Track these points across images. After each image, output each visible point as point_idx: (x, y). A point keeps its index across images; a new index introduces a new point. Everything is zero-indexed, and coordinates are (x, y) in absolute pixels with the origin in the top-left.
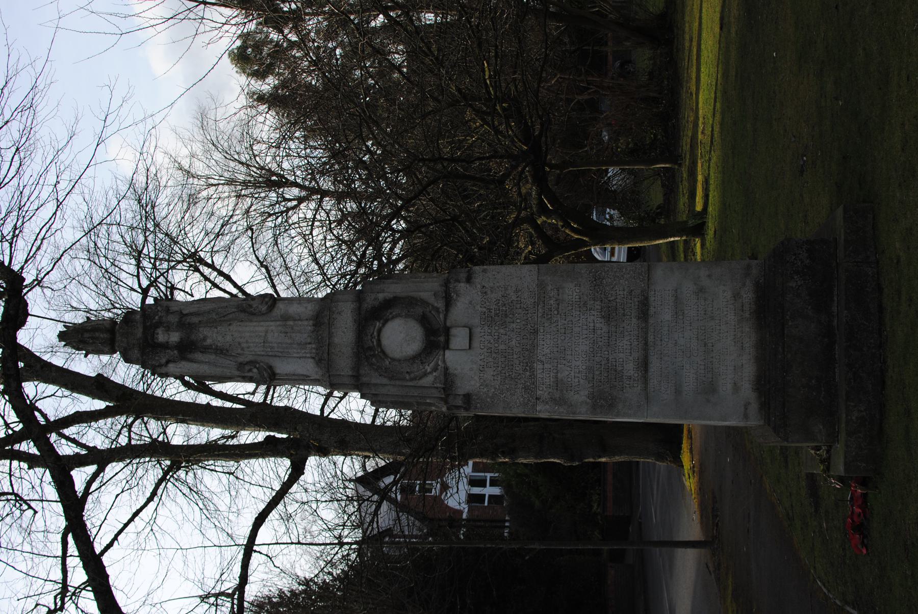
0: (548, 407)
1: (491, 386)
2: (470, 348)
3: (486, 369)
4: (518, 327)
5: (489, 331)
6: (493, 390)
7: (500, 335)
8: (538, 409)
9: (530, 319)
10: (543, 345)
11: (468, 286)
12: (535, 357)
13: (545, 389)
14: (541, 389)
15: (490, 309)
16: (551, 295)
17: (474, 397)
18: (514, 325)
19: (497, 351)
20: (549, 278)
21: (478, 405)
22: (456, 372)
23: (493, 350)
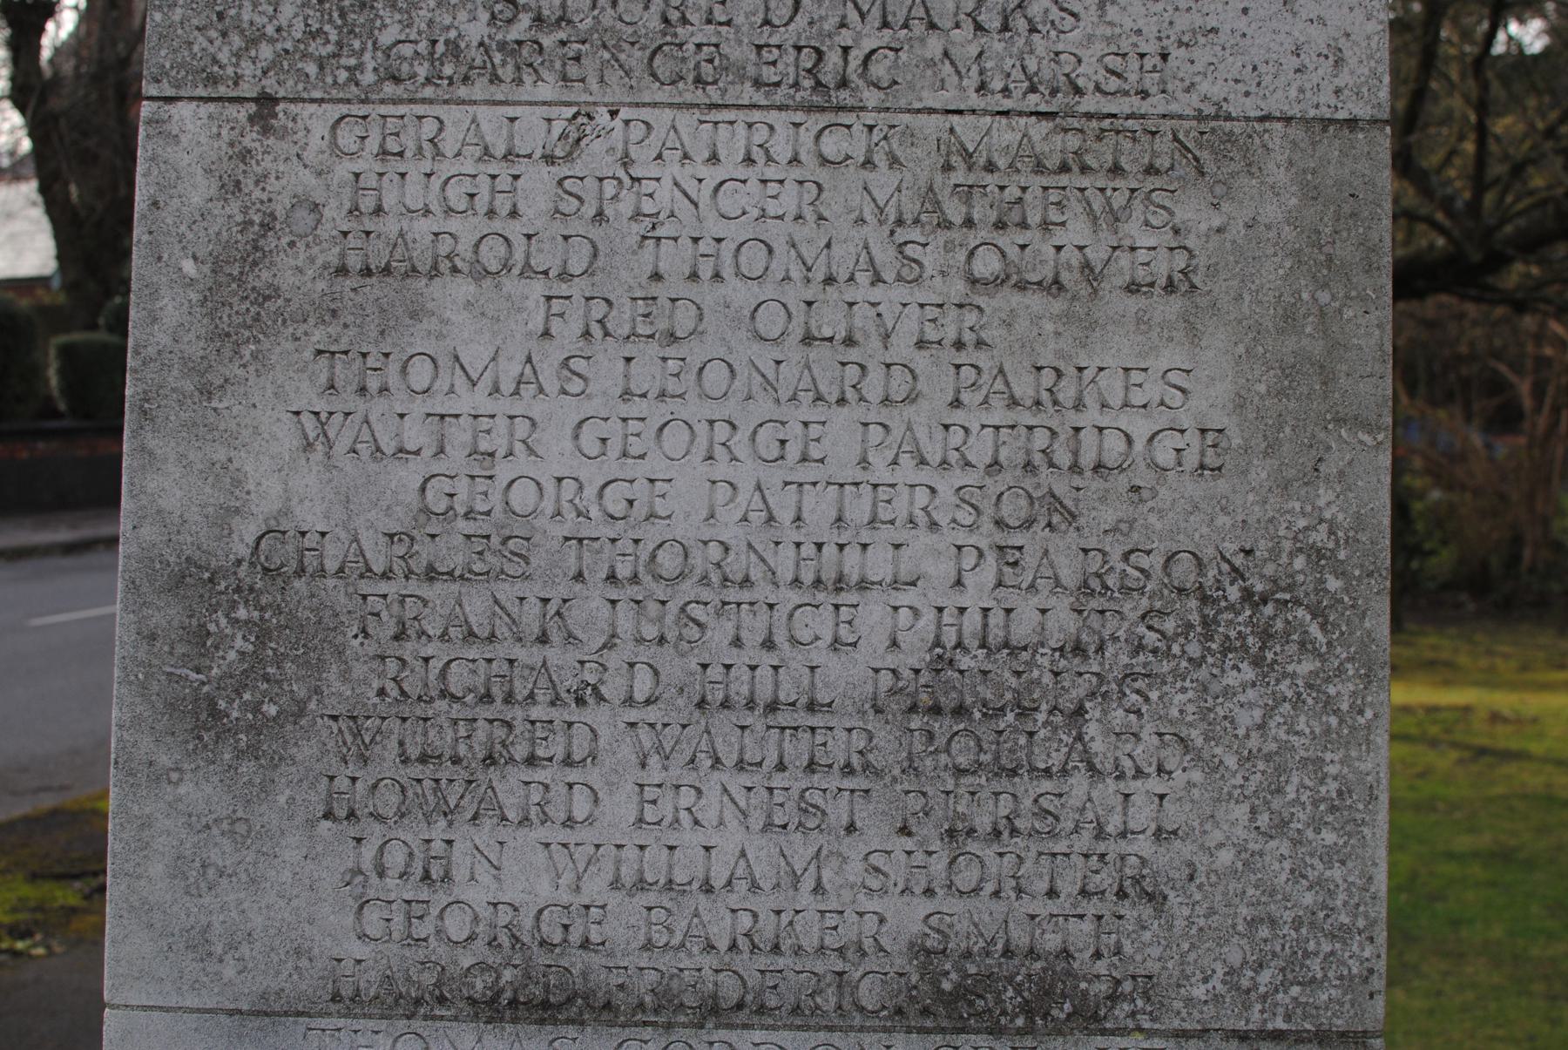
0: (196, 199)
8: (183, 110)
9: (934, 45)
10: (714, 158)
12: (616, 94)
13: (344, 169)
14: (347, 139)
16: (1133, 230)
20: (1271, 212)
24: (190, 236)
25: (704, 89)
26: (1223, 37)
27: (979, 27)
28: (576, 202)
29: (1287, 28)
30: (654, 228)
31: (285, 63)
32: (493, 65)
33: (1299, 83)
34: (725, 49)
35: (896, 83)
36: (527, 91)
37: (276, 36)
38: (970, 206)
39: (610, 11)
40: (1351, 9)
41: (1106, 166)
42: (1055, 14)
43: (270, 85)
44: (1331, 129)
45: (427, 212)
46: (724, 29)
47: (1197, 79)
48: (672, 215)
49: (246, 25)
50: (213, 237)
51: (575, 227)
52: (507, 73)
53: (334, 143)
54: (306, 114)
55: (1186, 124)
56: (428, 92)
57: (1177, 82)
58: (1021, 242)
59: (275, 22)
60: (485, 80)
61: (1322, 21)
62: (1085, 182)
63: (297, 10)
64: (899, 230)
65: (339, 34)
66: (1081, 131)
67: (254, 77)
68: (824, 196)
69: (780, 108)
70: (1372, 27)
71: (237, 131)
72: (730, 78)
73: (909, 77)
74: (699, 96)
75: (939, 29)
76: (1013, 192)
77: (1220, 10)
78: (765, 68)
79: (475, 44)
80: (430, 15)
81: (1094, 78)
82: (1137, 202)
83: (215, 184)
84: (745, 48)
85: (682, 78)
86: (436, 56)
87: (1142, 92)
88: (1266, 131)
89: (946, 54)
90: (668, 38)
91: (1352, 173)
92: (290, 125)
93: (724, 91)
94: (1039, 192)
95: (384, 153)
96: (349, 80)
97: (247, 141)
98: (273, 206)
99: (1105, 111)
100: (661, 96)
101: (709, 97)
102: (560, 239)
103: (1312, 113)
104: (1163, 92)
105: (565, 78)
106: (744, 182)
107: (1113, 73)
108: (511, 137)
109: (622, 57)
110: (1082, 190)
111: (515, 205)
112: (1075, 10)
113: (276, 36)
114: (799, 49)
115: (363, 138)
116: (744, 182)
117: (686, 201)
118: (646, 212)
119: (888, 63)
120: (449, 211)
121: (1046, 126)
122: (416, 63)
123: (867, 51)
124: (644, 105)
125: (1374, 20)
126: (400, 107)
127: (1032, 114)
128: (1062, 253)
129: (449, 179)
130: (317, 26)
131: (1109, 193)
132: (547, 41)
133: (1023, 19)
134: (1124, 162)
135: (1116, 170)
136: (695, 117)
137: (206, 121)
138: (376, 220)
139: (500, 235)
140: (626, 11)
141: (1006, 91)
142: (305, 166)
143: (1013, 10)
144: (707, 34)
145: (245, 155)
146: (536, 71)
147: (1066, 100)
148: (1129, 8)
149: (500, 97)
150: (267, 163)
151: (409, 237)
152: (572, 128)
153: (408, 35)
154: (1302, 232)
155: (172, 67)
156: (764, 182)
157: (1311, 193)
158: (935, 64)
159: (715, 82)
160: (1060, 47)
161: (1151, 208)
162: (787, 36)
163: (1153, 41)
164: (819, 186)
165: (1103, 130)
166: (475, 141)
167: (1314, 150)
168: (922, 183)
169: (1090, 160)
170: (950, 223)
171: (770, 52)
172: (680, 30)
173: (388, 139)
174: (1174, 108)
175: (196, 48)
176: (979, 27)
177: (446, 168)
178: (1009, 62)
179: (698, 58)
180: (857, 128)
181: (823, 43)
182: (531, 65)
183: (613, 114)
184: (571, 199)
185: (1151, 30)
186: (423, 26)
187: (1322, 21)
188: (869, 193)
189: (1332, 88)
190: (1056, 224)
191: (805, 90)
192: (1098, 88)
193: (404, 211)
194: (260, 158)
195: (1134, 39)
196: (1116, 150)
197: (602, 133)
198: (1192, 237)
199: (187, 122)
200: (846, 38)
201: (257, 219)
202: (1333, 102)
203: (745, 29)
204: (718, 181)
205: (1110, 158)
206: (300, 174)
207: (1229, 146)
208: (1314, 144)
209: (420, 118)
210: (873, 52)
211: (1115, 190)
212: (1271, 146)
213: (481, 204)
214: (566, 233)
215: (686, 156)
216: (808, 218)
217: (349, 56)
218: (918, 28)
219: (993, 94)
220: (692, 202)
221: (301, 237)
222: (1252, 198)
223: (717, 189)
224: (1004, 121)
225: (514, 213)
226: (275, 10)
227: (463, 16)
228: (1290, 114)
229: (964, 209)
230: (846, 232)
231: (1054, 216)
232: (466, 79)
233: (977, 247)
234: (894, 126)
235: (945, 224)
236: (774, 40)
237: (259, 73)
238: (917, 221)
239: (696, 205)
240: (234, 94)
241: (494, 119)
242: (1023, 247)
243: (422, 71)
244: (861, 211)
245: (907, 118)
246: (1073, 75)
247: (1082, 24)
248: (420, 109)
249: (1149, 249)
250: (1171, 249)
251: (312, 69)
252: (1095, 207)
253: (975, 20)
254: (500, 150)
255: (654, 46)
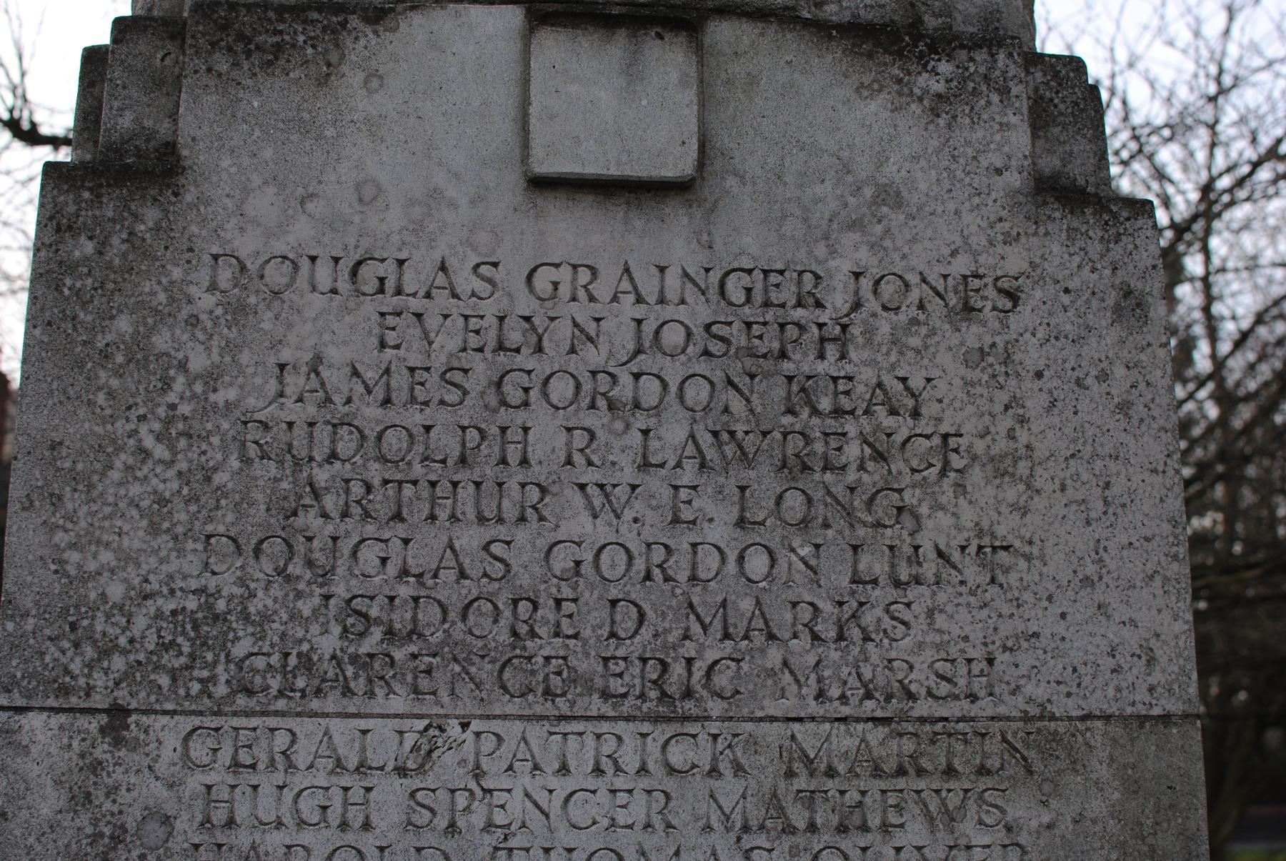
0: (46, 811)
1: (231, 348)
2: (541, 184)
3: (370, 307)
4: (709, 562)
5: (673, 336)
6: (198, 362)
7: (641, 421)
8: (34, 721)
9: (774, 656)
10: (564, 769)
11: (1014, 179)
12: (467, 706)
13: (195, 782)
14: (199, 751)
15: (843, 341)
16: (967, 828)
17: (152, 215)
18: (720, 531)
19: (514, 396)
20: (1096, 806)
21: (89, 247)
22: (357, 79)
23: (525, 360)
24: (38, 848)
25: (553, 701)
26: (1044, 641)
27: (815, 637)
28: (427, 814)
29: (1102, 631)
30: (506, 839)
31: (138, 675)
32: (345, 678)
33: (1115, 682)
34: (573, 662)
35: (738, 692)
36: (380, 703)
37: (128, 647)
38: (813, 811)
39: (460, 625)
40: (1159, 611)
41: (941, 768)
42: (887, 623)
43: (122, 695)
44: (1148, 724)
45: (279, 824)
46: (572, 642)
47: (1022, 682)
48: (524, 825)
49: (98, 636)
50: (62, 849)
51: (428, 839)
52: (359, 685)
53: (186, 755)
54: (158, 726)
55: (1014, 725)
56: (281, 704)
57: (1004, 686)
58: (863, 845)
59: (128, 633)
60: (338, 692)
61: (1133, 623)
62: (922, 785)
63: (150, 622)
64: (745, 836)
65: (191, 646)
66: (916, 735)
67: (106, 688)
68: (671, 804)
69: (628, 719)
70: (1179, 627)
71: (88, 742)
72: (579, 690)
73: (751, 687)
74: (549, 707)
75: (777, 639)
76: (853, 796)
77: (1040, 615)
78: (612, 680)
79: (327, 657)
80: (282, 628)
81: (926, 683)
82: (971, 802)
83: (65, 797)
84: (592, 660)
85: (531, 690)
86: (289, 669)
87: (971, 695)
88: (1088, 729)
89: (785, 663)
90: (518, 652)
91: (1169, 766)
92: (142, 736)
93: (573, 704)
94: (878, 796)
95: (236, 765)
96: (202, 692)
97: (98, 753)
98: (124, 818)
99: (937, 715)
100: (511, 709)
101: (558, 708)
102: (412, 850)
103: (1129, 710)
104: (991, 694)
105: (416, 690)
106: (594, 792)
107: (943, 678)
108: (363, 749)
109: (473, 670)
110: (918, 792)
111: (367, 817)
112: (906, 619)
113: (128, 647)
114: (644, 660)
115: (215, 750)
116: (594, 792)
117: (537, 811)
118: (498, 823)
119: (730, 673)
120: (302, 823)
121: (882, 731)
122: (269, 676)
123: (710, 662)
124: (495, 717)
125: (1180, 621)
126: (253, 719)
127: (869, 719)
128: (902, 854)
129: (302, 791)
130: (170, 638)
131: (944, 794)
132: (399, 655)
133: (857, 629)
134: (957, 763)
135: (950, 772)
136: (545, 729)
137: (57, 732)
138: (228, 832)
139: (353, 848)
140: (476, 625)
141: (843, 698)
142: (157, 778)
143: (848, 620)
144: (554, 646)
145: (96, 766)
146: (387, 684)
147: (900, 706)
148: (956, 616)
149: (352, 710)
150: (118, 774)
151: (261, 850)
152: (424, 740)
153: (261, 647)
154: (1126, 824)
155: (23, 677)
156: (613, 792)
157: (1132, 787)
158: (775, 674)
159: (564, 694)
160: (893, 654)
161: (984, 807)
162: (632, 648)
163: (979, 647)
164: (668, 796)
165: (936, 734)
166: (327, 753)
167: (1133, 746)
168: (766, 789)
169: (925, 763)
170: (795, 828)
171: (617, 664)
172: (529, 643)
173: (240, 751)
174: (1002, 710)
175: (48, 659)
176: (815, 637)
177: (299, 781)
178: (846, 670)
179: (546, 670)
180: (703, 737)
181: (667, 654)
182: (382, 678)
183: (465, 726)
184: (423, 811)
185: (977, 635)
186: (276, 639)
187: (1133, 623)
188: (716, 801)
189: (1146, 686)
190: (896, 826)
191: (651, 700)
192: (930, 693)
193: (257, 824)
194: (111, 769)
195: (962, 645)
196: (949, 752)
197: (454, 745)
198: (1024, 833)
199: (37, 732)
200: (689, 649)
201: (107, 831)
202: (1147, 699)
203: (592, 642)
204: (568, 792)
205: (943, 760)
206: (152, 786)
207: (1054, 745)
208: (1132, 740)
209: (272, 730)
210: (716, 662)
211: (949, 791)
212: (1093, 743)
213: (334, 816)
214: (418, 845)
215: (536, 767)
216: (657, 826)
217: (201, 668)
218: (758, 639)
219: (831, 700)
220: (543, 812)
221: (152, 849)
222: (1077, 795)
223: (567, 800)
224: (843, 727)
225: (367, 826)
226: (128, 622)
227: (315, 629)
228: (1109, 712)
229: (807, 814)
230: (693, 840)
231: (893, 818)
232: (318, 692)
233: (821, 851)
234: (738, 735)
235: (790, 830)
236: (620, 653)
237: (111, 684)
238: (762, 827)
239: (547, 816)
240: (86, 705)
241: (347, 732)
242: (864, 849)
243: (275, 683)
244: (708, 818)
245: (749, 726)
246: (906, 681)
247: (912, 632)
248: (272, 722)
249: (984, 847)
250: (1005, 846)
251: (164, 681)
252: (932, 808)
253: (812, 631)
254: (352, 763)
255: (503, 660)
